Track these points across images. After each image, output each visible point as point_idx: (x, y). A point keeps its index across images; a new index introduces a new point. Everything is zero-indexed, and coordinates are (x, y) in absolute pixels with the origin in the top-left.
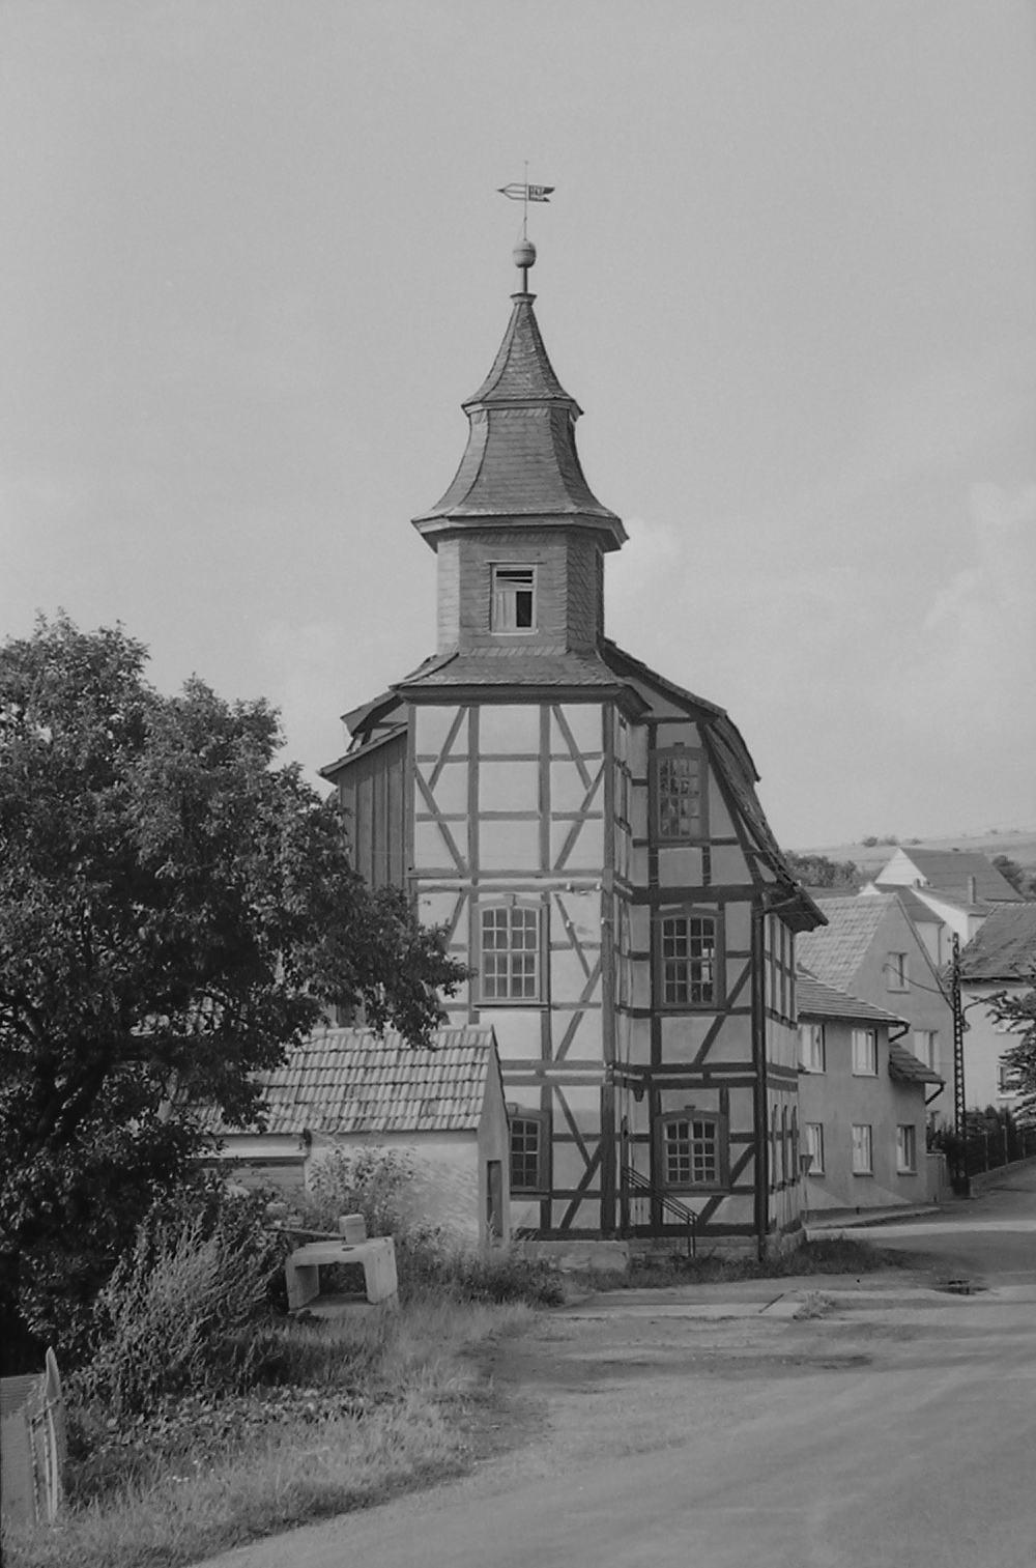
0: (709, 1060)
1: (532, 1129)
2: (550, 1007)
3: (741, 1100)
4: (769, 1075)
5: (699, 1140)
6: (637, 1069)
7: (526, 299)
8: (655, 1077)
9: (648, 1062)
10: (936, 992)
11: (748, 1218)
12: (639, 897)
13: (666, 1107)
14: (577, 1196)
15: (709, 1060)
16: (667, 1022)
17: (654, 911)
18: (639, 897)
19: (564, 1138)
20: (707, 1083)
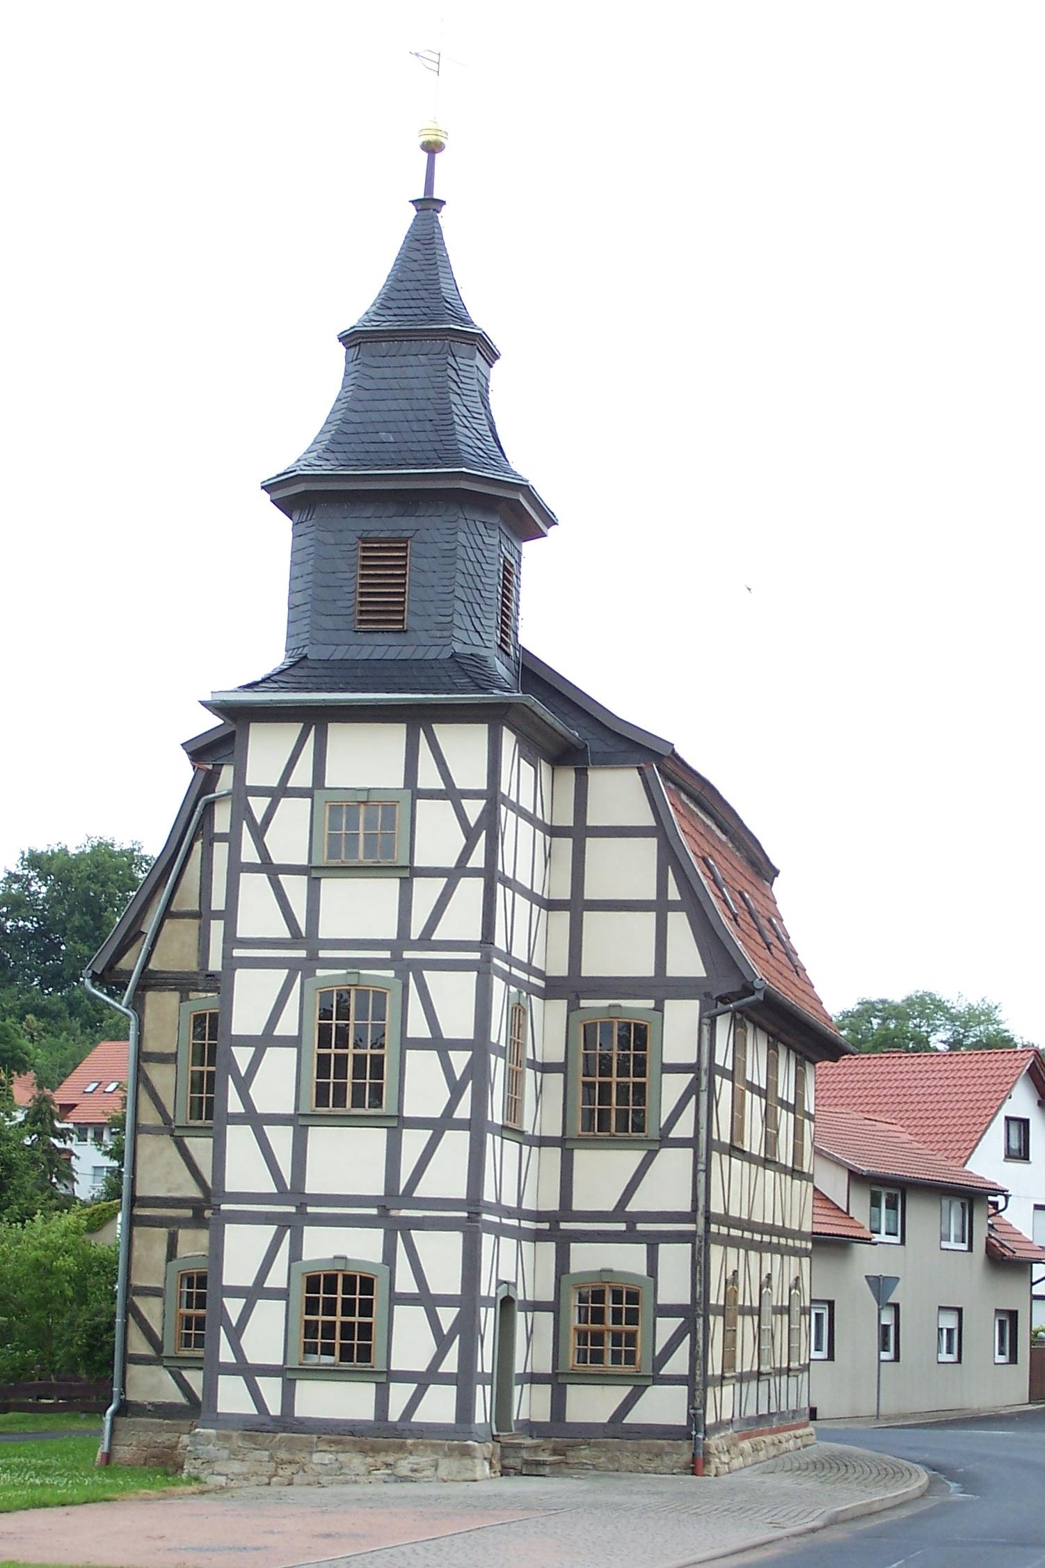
0: (632, 1207)
1: (368, 1285)
2: (399, 1117)
3: (676, 1259)
4: (714, 1228)
5: (617, 1327)
6: (538, 1216)
7: (428, 206)
8: (563, 1226)
9: (555, 1207)
10: (370, 655)
11: (678, 1417)
12: (553, 989)
13: (577, 1266)
14: (424, 1380)
15: (632, 1207)
16: (580, 1156)
17: (573, 1008)
18: (553, 989)
19: (420, 1044)
20: (630, 1236)
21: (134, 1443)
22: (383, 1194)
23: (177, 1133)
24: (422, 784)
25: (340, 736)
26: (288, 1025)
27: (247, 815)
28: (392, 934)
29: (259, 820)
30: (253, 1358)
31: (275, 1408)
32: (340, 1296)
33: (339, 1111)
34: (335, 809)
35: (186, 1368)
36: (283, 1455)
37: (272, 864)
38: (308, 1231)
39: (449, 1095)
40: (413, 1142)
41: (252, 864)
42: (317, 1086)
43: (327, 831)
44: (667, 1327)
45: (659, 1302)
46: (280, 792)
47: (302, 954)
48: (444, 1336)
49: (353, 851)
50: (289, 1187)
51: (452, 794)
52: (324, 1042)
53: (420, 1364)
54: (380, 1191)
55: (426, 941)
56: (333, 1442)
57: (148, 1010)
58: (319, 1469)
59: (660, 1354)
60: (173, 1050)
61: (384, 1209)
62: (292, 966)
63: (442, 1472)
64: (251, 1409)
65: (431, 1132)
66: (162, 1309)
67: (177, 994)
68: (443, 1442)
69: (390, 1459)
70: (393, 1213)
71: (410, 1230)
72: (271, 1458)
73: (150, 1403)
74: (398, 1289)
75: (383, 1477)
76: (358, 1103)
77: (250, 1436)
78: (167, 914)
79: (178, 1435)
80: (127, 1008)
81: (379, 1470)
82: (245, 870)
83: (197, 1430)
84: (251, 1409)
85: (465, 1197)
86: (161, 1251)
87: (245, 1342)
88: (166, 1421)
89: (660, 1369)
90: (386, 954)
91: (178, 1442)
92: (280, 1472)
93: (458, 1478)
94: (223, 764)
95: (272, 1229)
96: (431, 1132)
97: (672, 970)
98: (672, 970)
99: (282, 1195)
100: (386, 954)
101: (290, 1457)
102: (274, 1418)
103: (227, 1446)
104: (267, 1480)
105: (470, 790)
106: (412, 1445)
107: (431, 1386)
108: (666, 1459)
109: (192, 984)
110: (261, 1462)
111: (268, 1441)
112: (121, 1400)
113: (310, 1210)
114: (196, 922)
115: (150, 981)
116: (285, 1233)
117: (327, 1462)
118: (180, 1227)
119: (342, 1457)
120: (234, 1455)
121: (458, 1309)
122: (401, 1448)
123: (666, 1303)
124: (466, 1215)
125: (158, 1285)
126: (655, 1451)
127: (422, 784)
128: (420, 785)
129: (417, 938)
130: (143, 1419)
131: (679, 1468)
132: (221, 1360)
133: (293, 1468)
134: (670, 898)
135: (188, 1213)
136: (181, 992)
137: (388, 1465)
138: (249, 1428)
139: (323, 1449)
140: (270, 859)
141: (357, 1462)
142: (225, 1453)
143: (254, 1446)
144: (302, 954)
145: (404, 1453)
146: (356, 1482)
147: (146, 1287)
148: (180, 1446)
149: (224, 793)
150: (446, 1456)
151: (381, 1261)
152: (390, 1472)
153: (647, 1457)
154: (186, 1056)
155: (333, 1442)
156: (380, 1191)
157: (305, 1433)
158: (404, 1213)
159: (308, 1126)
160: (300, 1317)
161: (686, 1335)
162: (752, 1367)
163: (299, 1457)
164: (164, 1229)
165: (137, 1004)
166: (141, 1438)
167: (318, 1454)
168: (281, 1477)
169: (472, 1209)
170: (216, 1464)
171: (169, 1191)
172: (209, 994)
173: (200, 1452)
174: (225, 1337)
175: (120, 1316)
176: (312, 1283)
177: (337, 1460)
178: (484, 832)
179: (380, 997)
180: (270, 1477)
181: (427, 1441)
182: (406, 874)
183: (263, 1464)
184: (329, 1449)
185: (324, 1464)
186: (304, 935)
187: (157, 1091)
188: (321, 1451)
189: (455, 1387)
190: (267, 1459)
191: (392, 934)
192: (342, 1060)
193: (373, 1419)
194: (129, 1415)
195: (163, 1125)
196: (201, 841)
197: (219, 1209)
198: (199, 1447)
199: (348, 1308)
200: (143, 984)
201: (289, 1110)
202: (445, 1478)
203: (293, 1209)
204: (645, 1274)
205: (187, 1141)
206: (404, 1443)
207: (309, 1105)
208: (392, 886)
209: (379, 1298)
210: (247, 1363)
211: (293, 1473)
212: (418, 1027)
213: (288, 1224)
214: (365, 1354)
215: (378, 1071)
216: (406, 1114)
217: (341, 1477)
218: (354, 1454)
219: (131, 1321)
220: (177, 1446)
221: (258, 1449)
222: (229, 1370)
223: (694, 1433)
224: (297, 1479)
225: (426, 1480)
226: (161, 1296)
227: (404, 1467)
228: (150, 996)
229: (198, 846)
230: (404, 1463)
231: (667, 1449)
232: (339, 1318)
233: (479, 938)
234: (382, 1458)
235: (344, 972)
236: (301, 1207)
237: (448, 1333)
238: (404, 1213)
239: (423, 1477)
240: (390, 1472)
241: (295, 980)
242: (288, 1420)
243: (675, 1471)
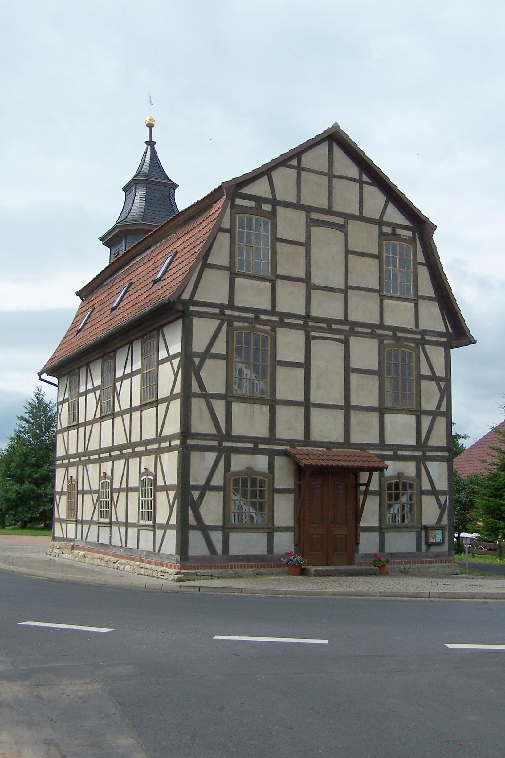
90: (301, 322)
176: (389, 487)
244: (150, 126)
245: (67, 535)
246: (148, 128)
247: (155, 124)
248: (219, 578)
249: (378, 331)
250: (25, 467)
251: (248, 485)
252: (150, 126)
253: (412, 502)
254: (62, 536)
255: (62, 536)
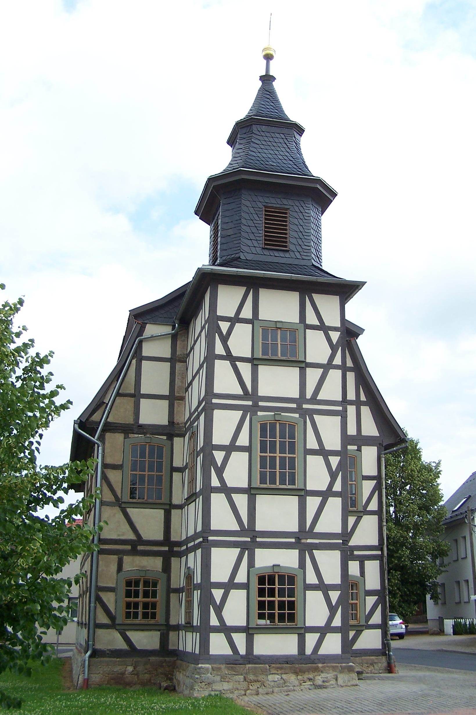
1: (292, 579)
19: (313, 452)
21: (101, 672)
22: (298, 531)
23: (123, 506)
24: (308, 322)
25: (265, 295)
26: (243, 440)
27: (218, 330)
28: (296, 395)
29: (224, 333)
30: (229, 622)
31: (242, 650)
32: (277, 586)
33: (273, 486)
34: (265, 331)
35: (128, 630)
36: (251, 677)
37: (232, 356)
38: (258, 552)
39: (330, 479)
40: (313, 503)
41: (222, 355)
42: (260, 473)
43: (261, 341)
44: (371, 601)
45: (366, 589)
46: (235, 320)
47: (250, 403)
48: (333, 606)
49: (275, 353)
50: (246, 527)
51: (322, 327)
52: (263, 449)
53: (321, 622)
54: (296, 529)
55: (314, 400)
56: (278, 668)
57: (107, 443)
58: (272, 684)
59: (368, 614)
60: (121, 463)
61: (298, 539)
62: (245, 409)
63: (340, 682)
64: (229, 651)
65: (321, 498)
66: (115, 599)
67: (123, 435)
68: (338, 665)
69: (311, 676)
70: (303, 541)
71: (312, 550)
72: (245, 679)
73: (108, 650)
74: (308, 582)
75: (309, 686)
76: (283, 482)
77: (232, 667)
78: (118, 394)
79: (125, 666)
80: (97, 440)
81: (305, 682)
82: (217, 358)
83: (200, 665)
84: (229, 651)
85: (341, 532)
86: (114, 567)
87: (226, 613)
88: (118, 659)
89: (368, 622)
90: (294, 406)
91: (125, 671)
92: (251, 687)
93: (349, 684)
94: (147, 323)
95: (237, 551)
96: (321, 498)
97: (364, 433)
98: (364, 433)
99: (242, 532)
100: (294, 406)
101: (256, 678)
102: (242, 656)
103: (219, 674)
104: (243, 693)
105: (333, 327)
106: (322, 667)
107: (328, 634)
108: (376, 666)
109: (130, 430)
110: (239, 682)
111: (242, 669)
112: (93, 649)
113: (258, 540)
114: (133, 399)
115: (109, 427)
116: (245, 552)
117: (276, 680)
118: (124, 555)
119: (284, 676)
120: (223, 679)
121: (340, 592)
122: (316, 669)
123: (370, 589)
124: (341, 541)
125: (113, 586)
126: (371, 662)
127: (308, 322)
128: (308, 322)
129: (310, 398)
130: (105, 659)
131: (382, 670)
132: (211, 624)
133: (258, 684)
134: (361, 400)
135: (129, 547)
136: (125, 434)
137: (310, 679)
138: (228, 663)
139: (273, 673)
140: (231, 353)
141: (292, 678)
142: (218, 678)
143: (234, 673)
144: (250, 403)
145: (318, 672)
146: (294, 690)
147: (105, 587)
148: (127, 673)
149: (150, 336)
150: (341, 672)
151: (298, 567)
152: (312, 683)
153: (367, 665)
154: (128, 466)
155: (278, 668)
156: (296, 529)
157: (262, 664)
158: (309, 541)
159: (256, 494)
160: (255, 598)
161: (379, 604)
162: (197, 624)
163: (260, 678)
164: (115, 556)
165: (102, 438)
166: (105, 669)
167: (271, 675)
168: (252, 690)
169: (345, 539)
170: (213, 685)
171: (119, 535)
172: (140, 436)
173: (203, 678)
174: (213, 610)
175: (93, 603)
176: (261, 580)
177: (282, 678)
178: (340, 347)
179: (292, 427)
180: (245, 691)
181: (329, 665)
182: (303, 365)
183: (240, 683)
184: (277, 672)
185: (275, 681)
186: (250, 394)
187: (112, 484)
188: (273, 674)
189: (340, 634)
190: (242, 680)
191: (296, 395)
192: (273, 459)
193: (297, 654)
194: (97, 656)
195: (115, 501)
196: (136, 359)
197: (208, 540)
198: (202, 676)
199: (282, 593)
200: (104, 429)
201: (245, 485)
202: (342, 684)
203: (249, 539)
204: (359, 576)
205: (128, 510)
206: (318, 666)
207: (256, 483)
208: (295, 372)
209: (299, 586)
210: (226, 625)
211: (258, 688)
212: (312, 443)
213: (247, 548)
214: (292, 618)
215: (292, 466)
216: (308, 488)
217: (285, 688)
218: (291, 675)
219: (98, 605)
220: (125, 673)
221: (237, 675)
222: (216, 630)
223: (387, 652)
224: (260, 690)
225: (332, 686)
226: (114, 592)
227: (319, 680)
228: (108, 435)
229: (134, 361)
230: (319, 678)
231: (376, 661)
232: (277, 599)
233: (341, 400)
234: (306, 676)
235: (273, 413)
236: (254, 538)
237: (335, 605)
238: (309, 541)
239: (330, 685)
240: (312, 683)
241: (247, 415)
242: (250, 657)
243: (380, 672)
244: (268, 57)
245: (186, 650)
246: (265, 61)
247: (274, 55)
248: (257, 681)
249: (199, 460)
250: (49, 558)
251: (283, 575)
252: (268, 57)
253: (353, 591)
254: (191, 651)
255: (191, 651)
